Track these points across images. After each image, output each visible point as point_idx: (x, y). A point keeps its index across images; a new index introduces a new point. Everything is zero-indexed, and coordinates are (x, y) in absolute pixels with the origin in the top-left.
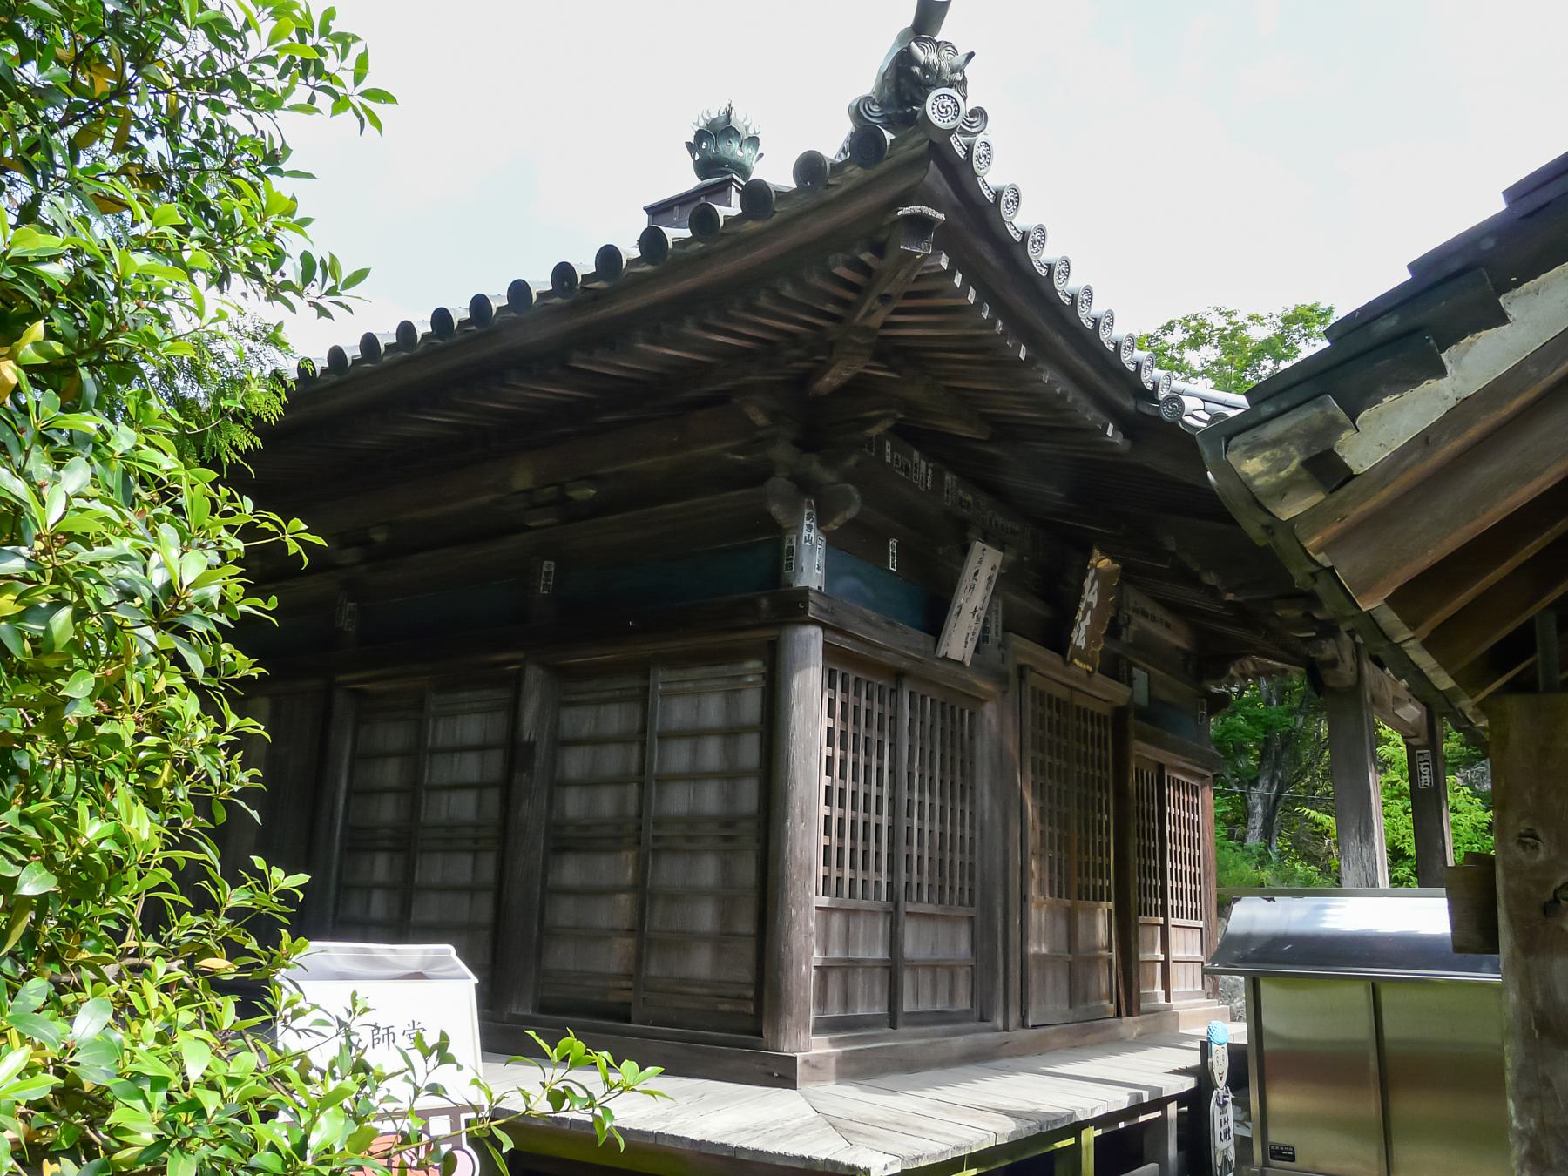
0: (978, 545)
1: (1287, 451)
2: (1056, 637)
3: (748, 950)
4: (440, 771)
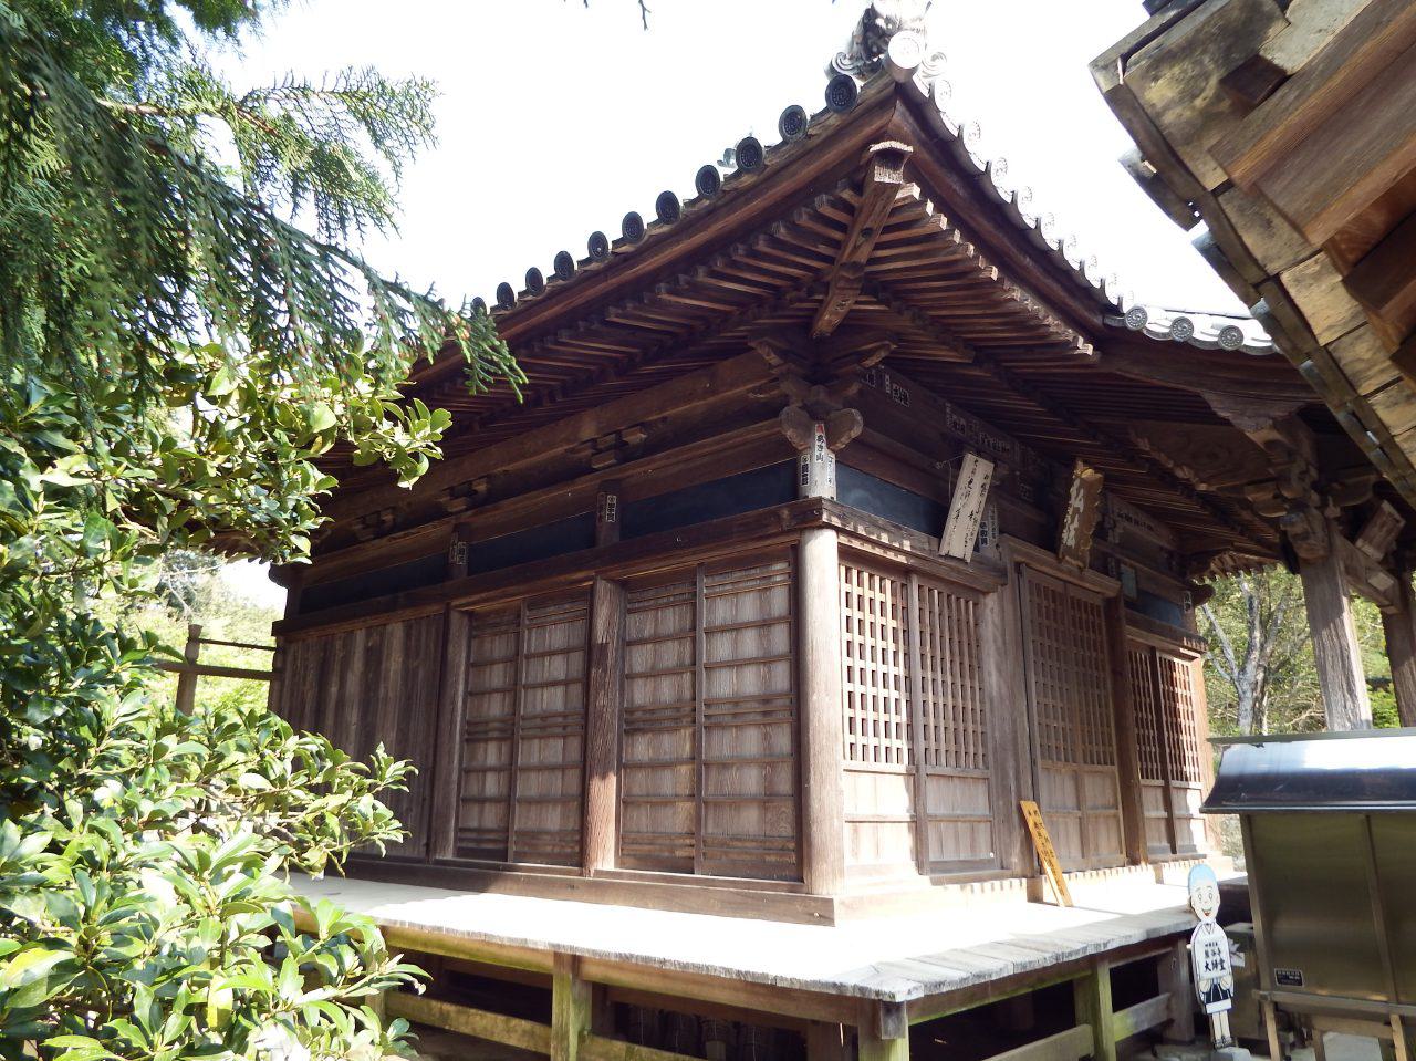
0: (970, 458)
1: (1201, 63)
2: (1048, 539)
3: (788, 809)
4: (533, 672)
